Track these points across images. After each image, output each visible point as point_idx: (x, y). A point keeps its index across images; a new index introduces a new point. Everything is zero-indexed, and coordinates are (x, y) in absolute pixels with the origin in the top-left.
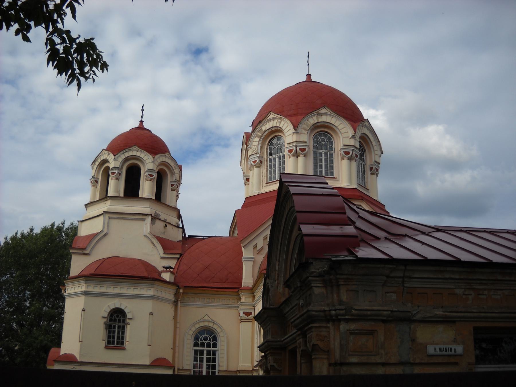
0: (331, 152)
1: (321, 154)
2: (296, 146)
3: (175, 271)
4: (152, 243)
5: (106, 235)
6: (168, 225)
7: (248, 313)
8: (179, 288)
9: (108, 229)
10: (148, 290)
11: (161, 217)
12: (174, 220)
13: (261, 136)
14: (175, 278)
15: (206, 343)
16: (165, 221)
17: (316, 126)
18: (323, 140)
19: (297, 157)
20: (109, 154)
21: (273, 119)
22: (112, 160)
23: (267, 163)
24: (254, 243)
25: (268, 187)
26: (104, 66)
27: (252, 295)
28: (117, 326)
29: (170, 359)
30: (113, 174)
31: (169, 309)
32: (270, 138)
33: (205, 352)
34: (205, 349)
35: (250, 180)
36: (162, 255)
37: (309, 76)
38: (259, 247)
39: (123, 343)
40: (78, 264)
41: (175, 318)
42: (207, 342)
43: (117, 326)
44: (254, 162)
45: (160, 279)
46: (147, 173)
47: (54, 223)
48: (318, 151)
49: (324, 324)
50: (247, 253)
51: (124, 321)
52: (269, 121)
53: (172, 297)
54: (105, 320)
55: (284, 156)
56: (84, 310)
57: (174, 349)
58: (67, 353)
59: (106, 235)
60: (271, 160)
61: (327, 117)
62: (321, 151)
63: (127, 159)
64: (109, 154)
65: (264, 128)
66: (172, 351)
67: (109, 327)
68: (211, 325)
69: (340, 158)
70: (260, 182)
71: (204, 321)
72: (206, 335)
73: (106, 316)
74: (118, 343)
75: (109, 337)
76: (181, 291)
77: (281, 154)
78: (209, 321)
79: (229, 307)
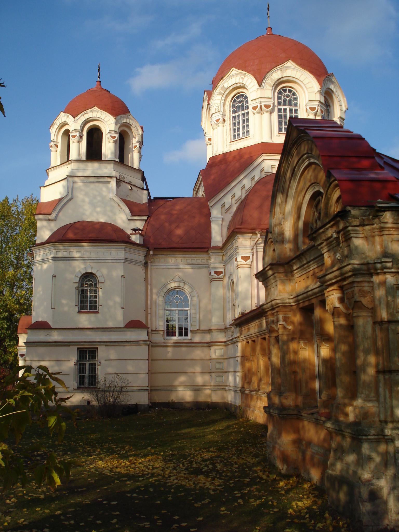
0: (296, 108)
1: (285, 110)
2: (260, 102)
3: (144, 233)
4: (119, 205)
5: (70, 200)
6: (133, 187)
8: (149, 250)
9: (72, 193)
11: (125, 180)
12: (139, 183)
14: (144, 239)
16: (130, 183)
17: (279, 82)
18: (287, 97)
19: (262, 114)
20: (68, 117)
22: (72, 122)
23: (230, 121)
24: (222, 202)
29: (144, 321)
30: (74, 137)
31: (140, 270)
36: (130, 218)
38: (227, 206)
39: (96, 307)
40: (44, 232)
41: (146, 279)
45: (129, 241)
46: (109, 135)
47: (7, 198)
48: (282, 107)
49: (367, 279)
50: (215, 212)
51: (96, 285)
52: (231, 77)
53: (141, 258)
54: (76, 285)
55: (248, 113)
56: (54, 276)
57: (146, 310)
58: (40, 320)
59: (70, 200)
60: (234, 117)
61: (291, 70)
62: (285, 107)
63: (87, 122)
64: (68, 117)
65: (226, 86)
66: (145, 312)
73: (78, 281)
74: (91, 307)
75: (81, 302)
77: (245, 112)
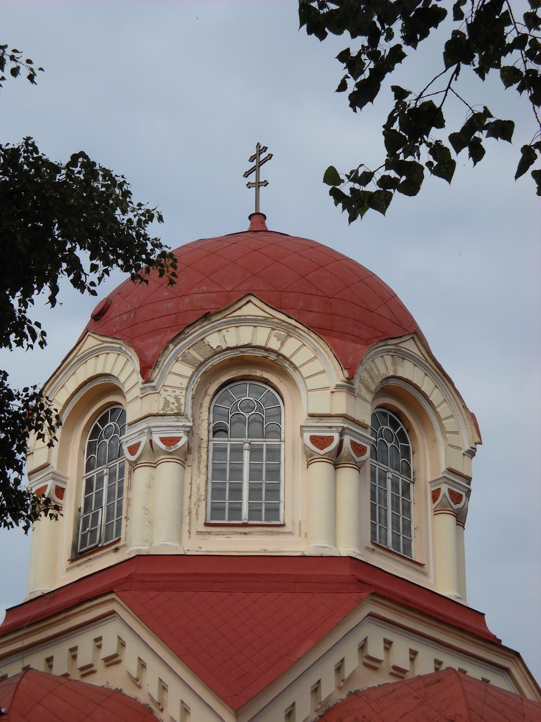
13: (202, 364)
19: (336, 466)
24: (311, 681)
25: (213, 538)
26: (352, 219)
32: (224, 379)
44: (169, 441)
65: (214, 340)
67: (463, 670)
70: (180, 517)
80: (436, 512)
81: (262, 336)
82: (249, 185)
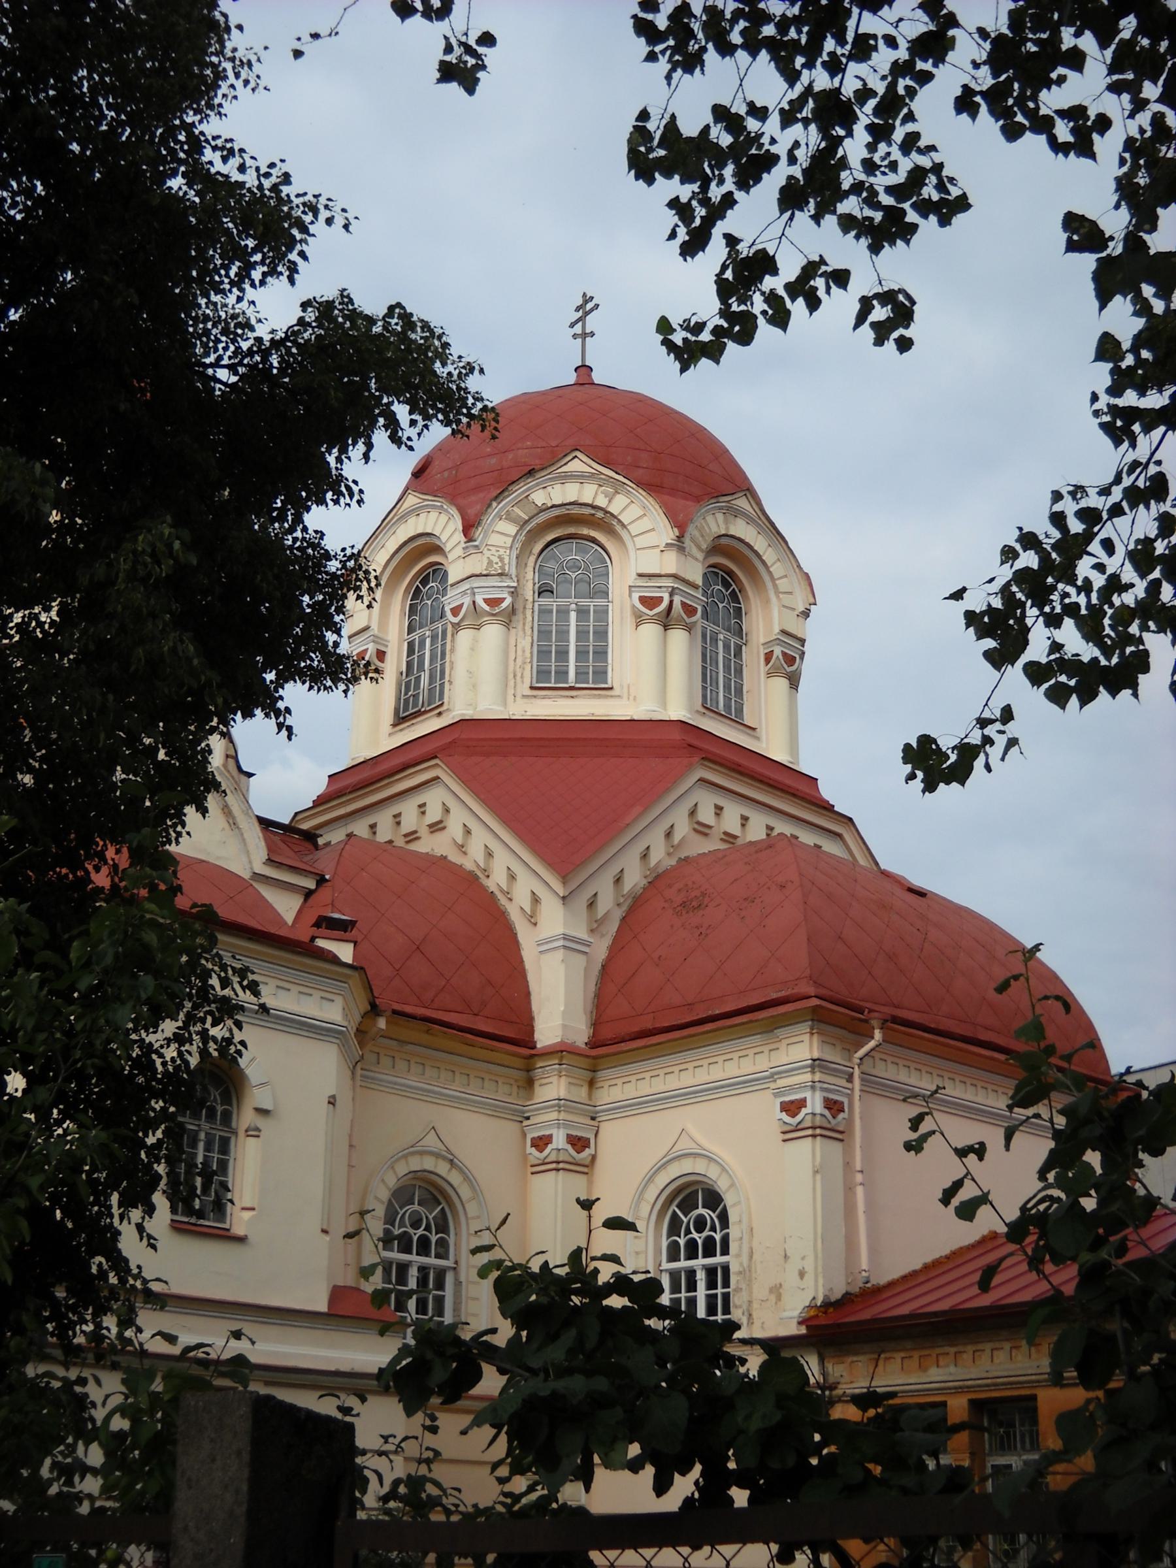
7: (580, 1139)
10: (326, 1004)
13: (526, 522)
15: (699, 1238)
21: (580, 478)
25: (539, 702)
27: (588, 1074)
28: (202, 1136)
33: (701, 1276)
34: (700, 1262)
35: (388, 657)
37: (584, 369)
42: (704, 1234)
43: (202, 1136)
62: (562, 601)
65: (539, 498)
68: (442, 1168)
69: (630, 621)
71: (421, 1153)
72: (416, 1207)
76: (382, 1023)
77: (591, 604)
78: (437, 1155)
79: (497, 1111)
80: (769, 675)
81: (588, 493)
82: (575, 336)
